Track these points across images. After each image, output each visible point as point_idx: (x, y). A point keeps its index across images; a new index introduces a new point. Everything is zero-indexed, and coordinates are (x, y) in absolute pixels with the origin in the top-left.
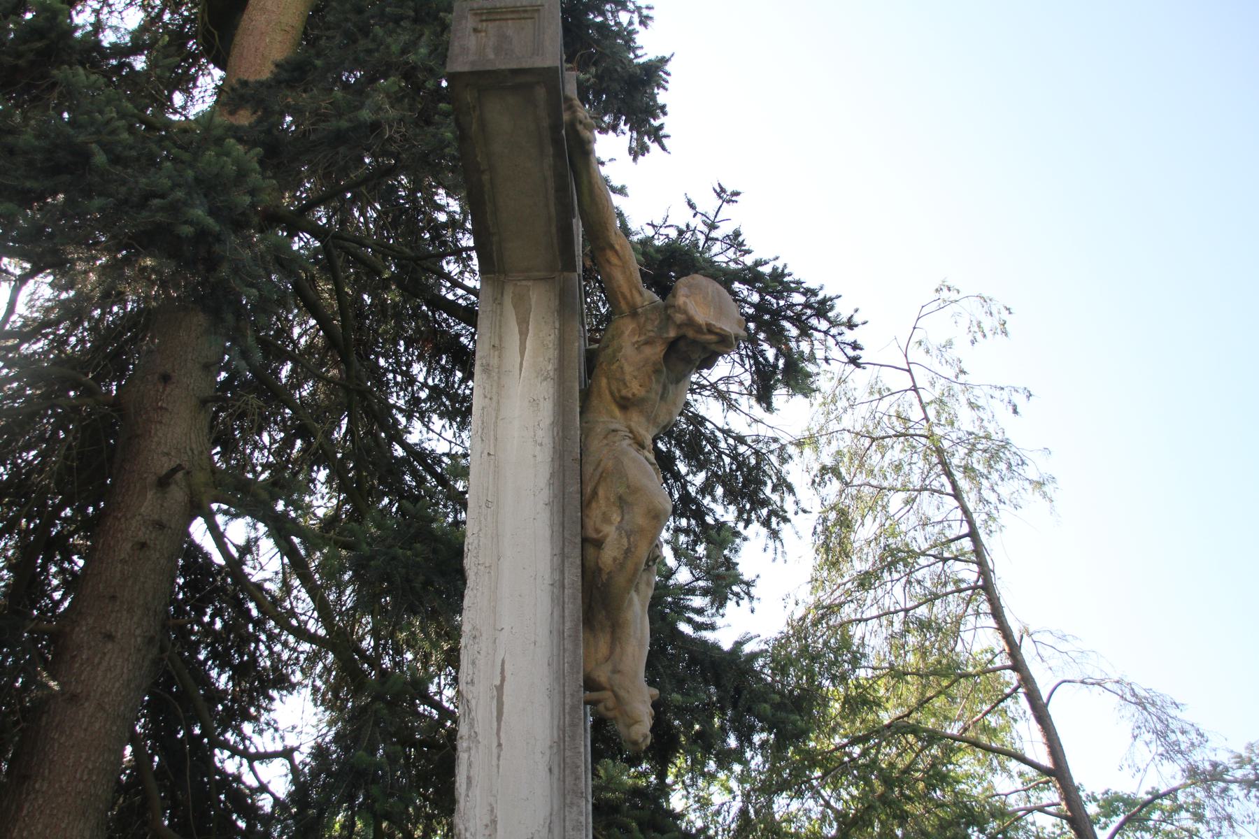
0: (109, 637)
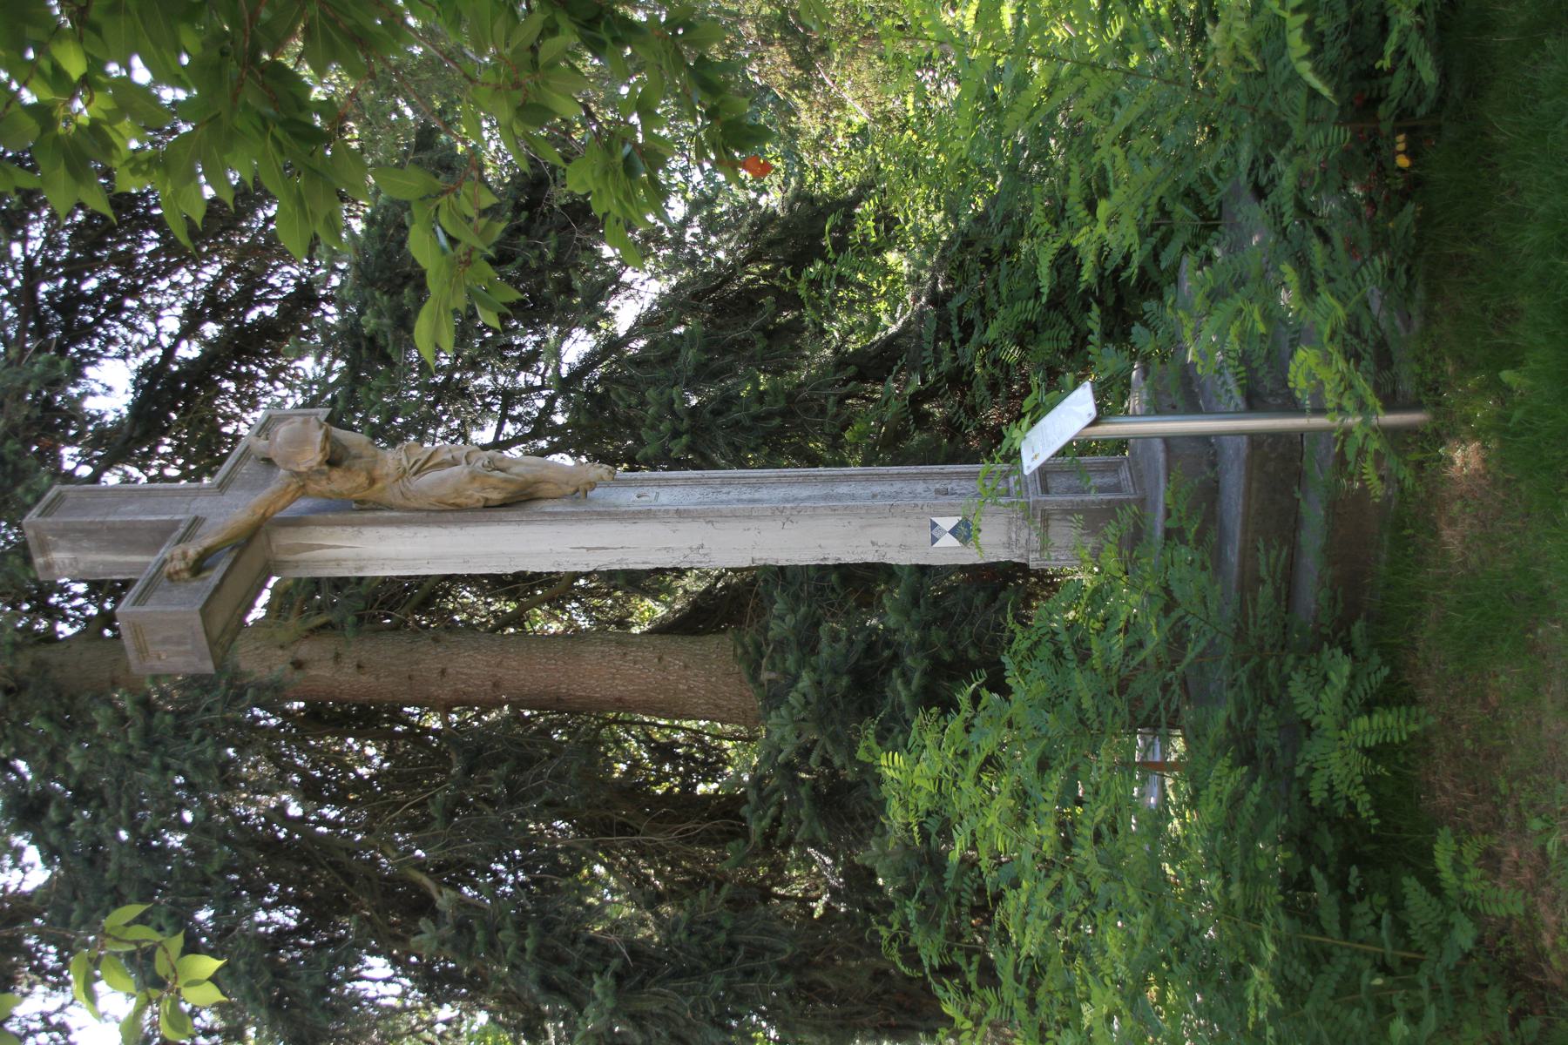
0: (443, 672)
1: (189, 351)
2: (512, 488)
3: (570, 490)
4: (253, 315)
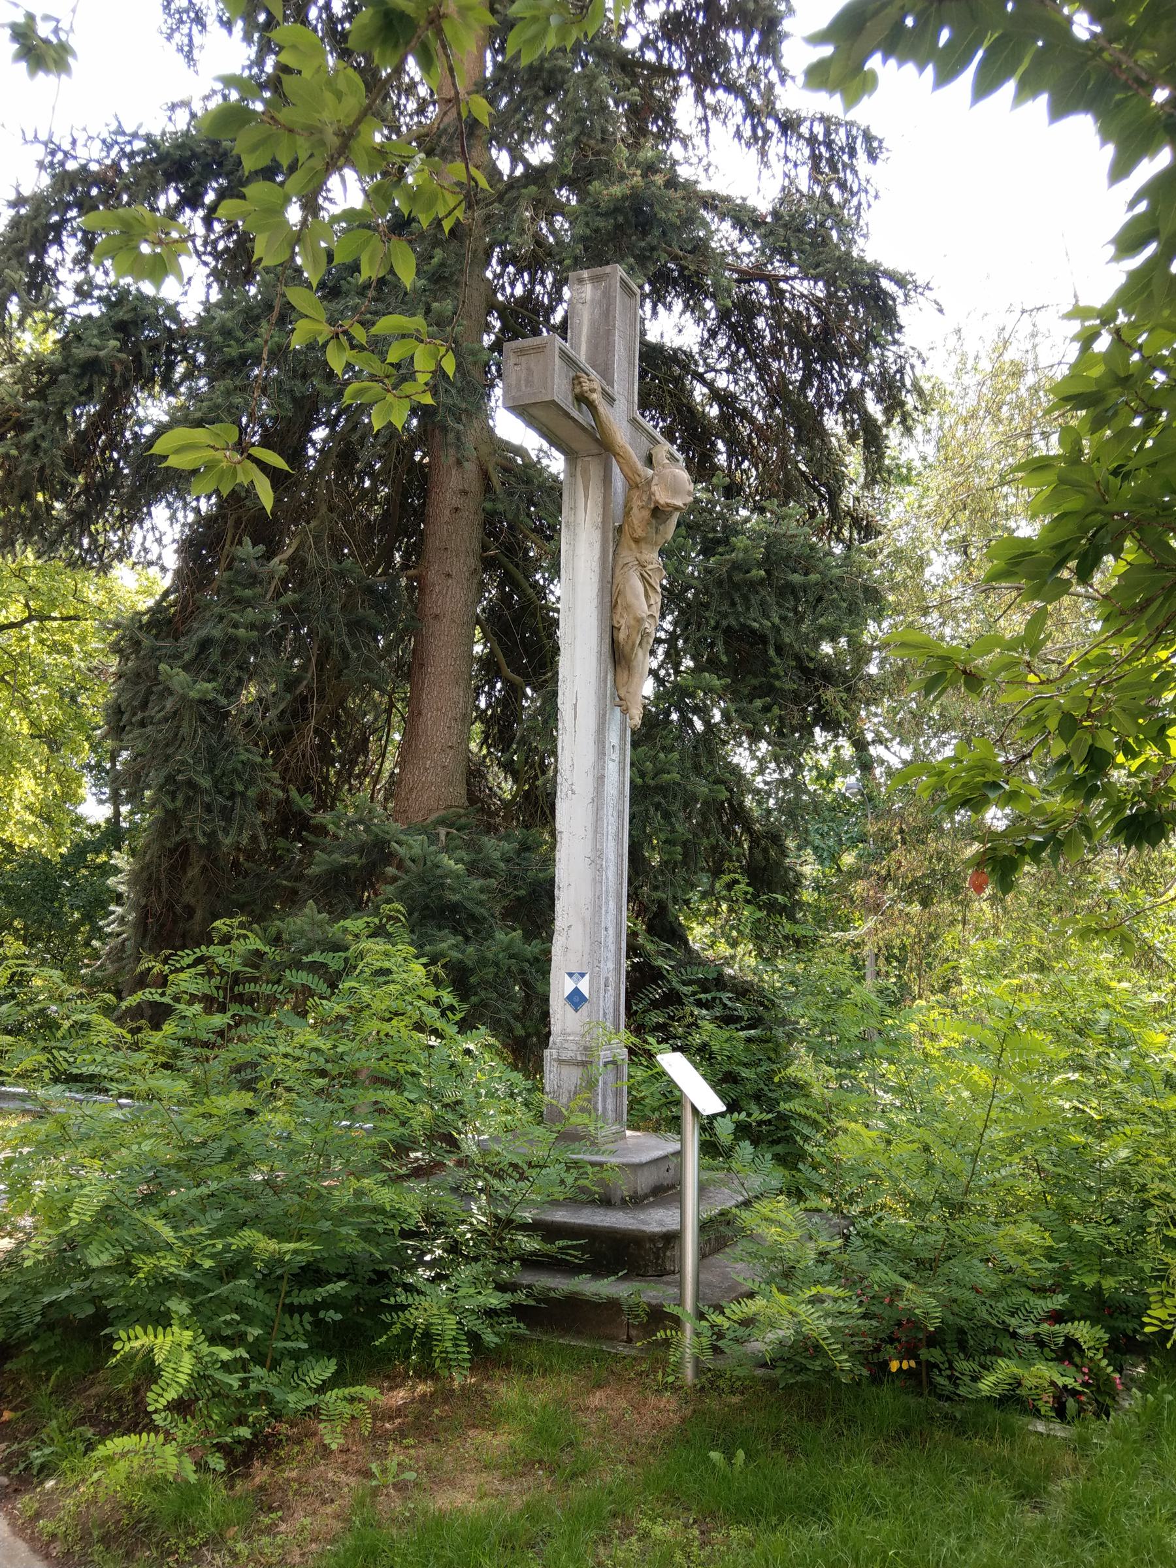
0: (449, 575)
1: (699, 392)
2: (627, 649)
3: (622, 693)
4: (721, 445)
